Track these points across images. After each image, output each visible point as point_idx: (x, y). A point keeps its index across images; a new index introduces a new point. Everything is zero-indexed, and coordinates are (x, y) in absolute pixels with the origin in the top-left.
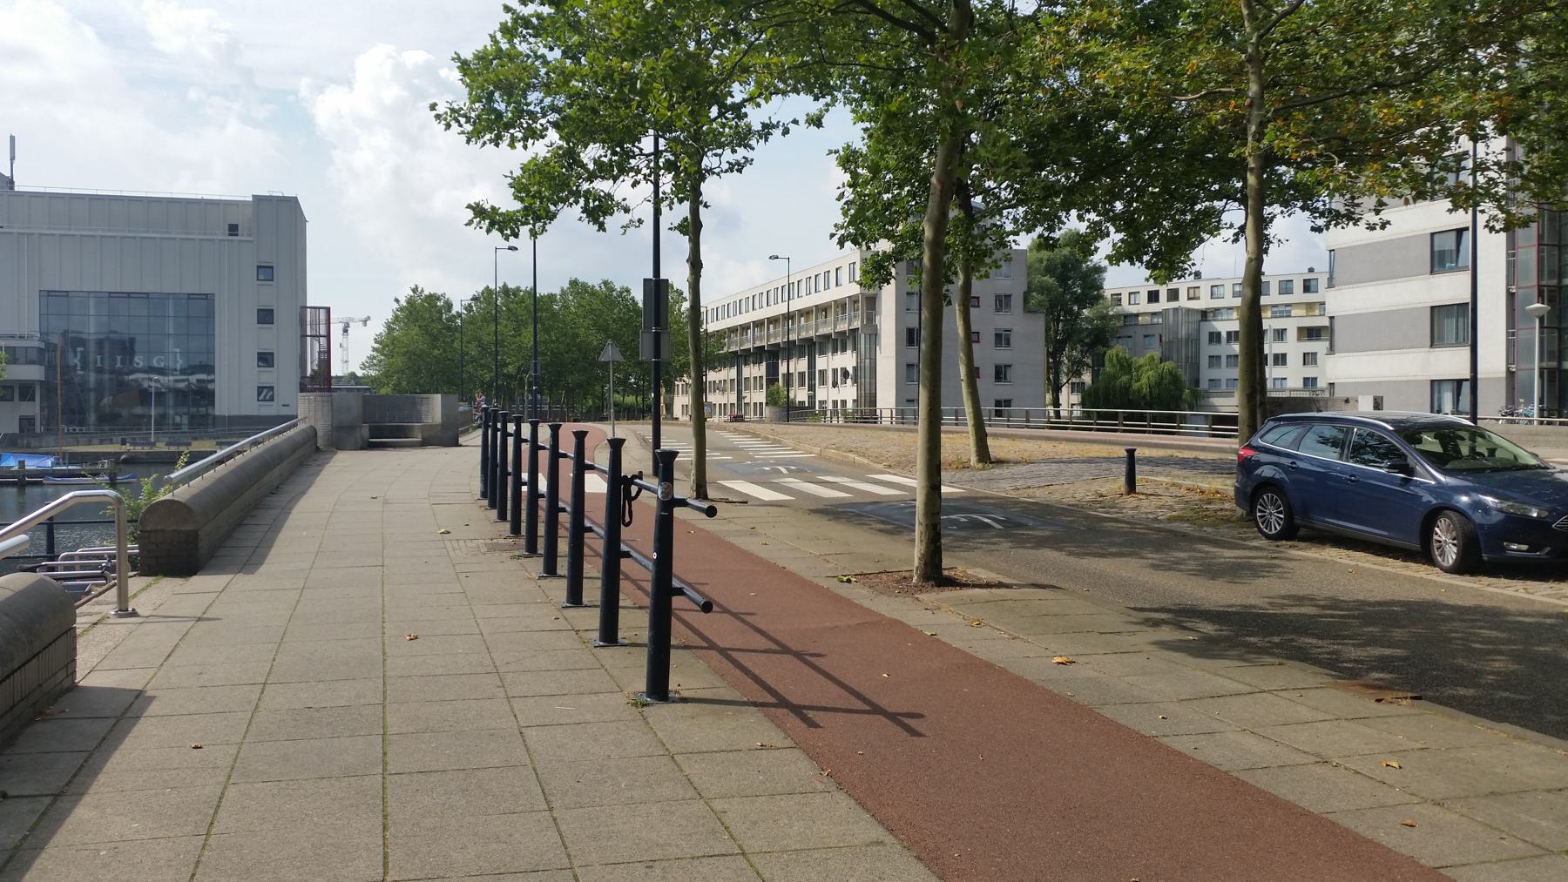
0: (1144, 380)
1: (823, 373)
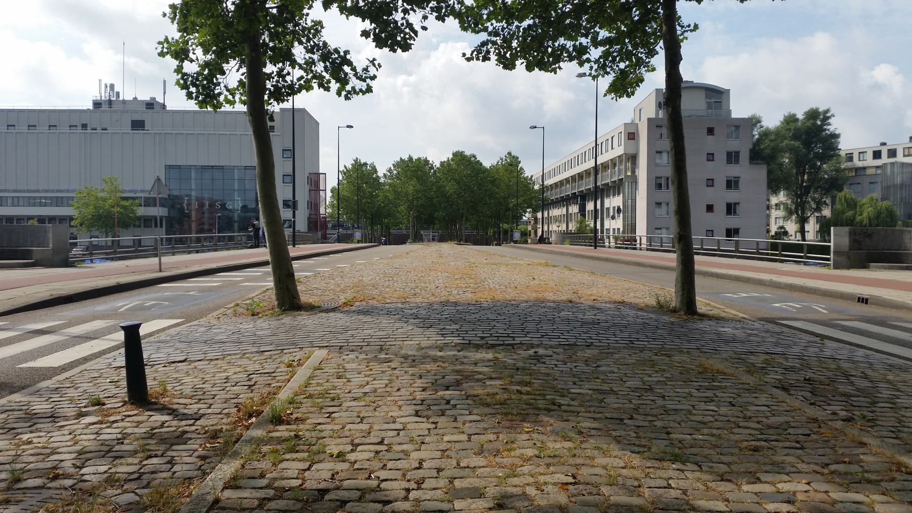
0: (865, 214)
1: (608, 209)
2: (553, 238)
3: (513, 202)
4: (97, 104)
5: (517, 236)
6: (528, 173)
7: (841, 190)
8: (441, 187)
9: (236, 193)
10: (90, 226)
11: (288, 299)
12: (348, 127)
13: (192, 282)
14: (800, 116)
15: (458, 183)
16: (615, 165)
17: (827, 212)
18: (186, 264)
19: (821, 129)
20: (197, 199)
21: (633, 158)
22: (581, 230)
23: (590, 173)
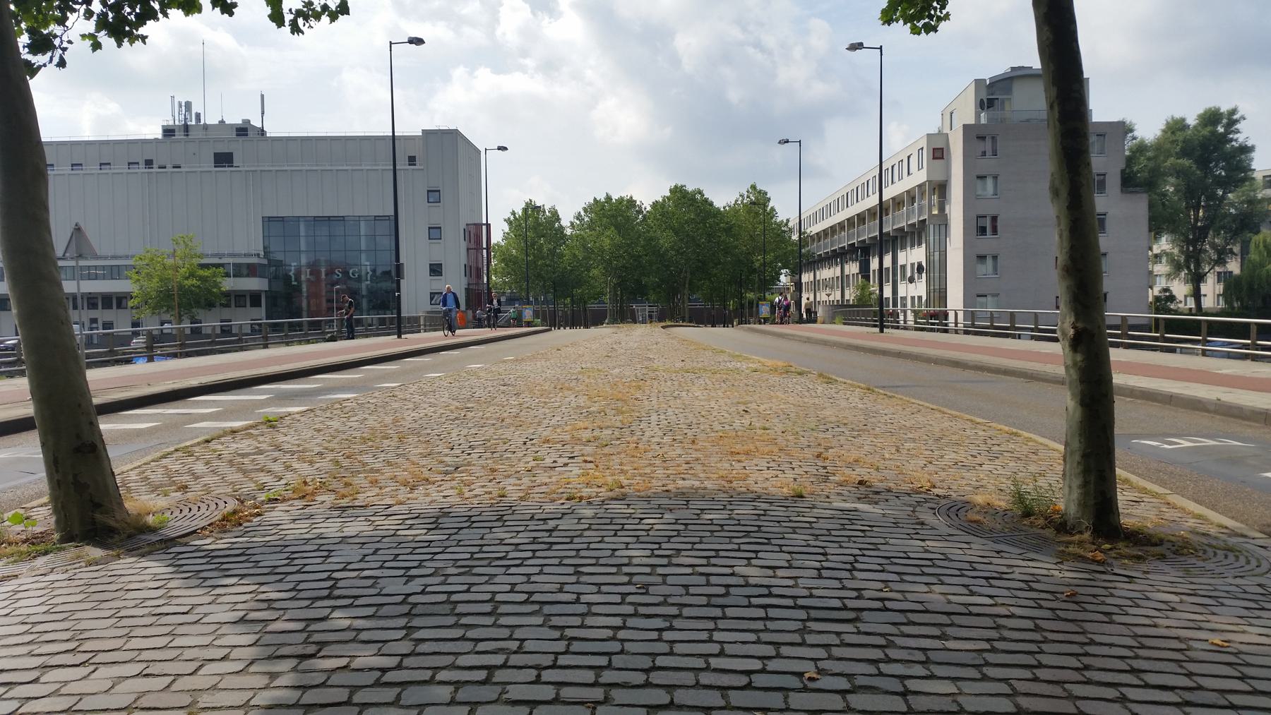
1: (903, 267)
2: (820, 312)
3: (758, 259)
4: (168, 132)
5: (765, 310)
6: (781, 216)
7: (1258, 232)
8: (651, 239)
9: (363, 256)
10: (156, 308)
11: (89, 510)
12: (499, 148)
13: (139, 419)
14: (1192, 121)
15: (676, 233)
16: (913, 200)
17: (1234, 267)
18: (149, 379)
19: (1224, 139)
20: (309, 265)
21: (941, 189)
22: (862, 301)
23: (875, 214)
